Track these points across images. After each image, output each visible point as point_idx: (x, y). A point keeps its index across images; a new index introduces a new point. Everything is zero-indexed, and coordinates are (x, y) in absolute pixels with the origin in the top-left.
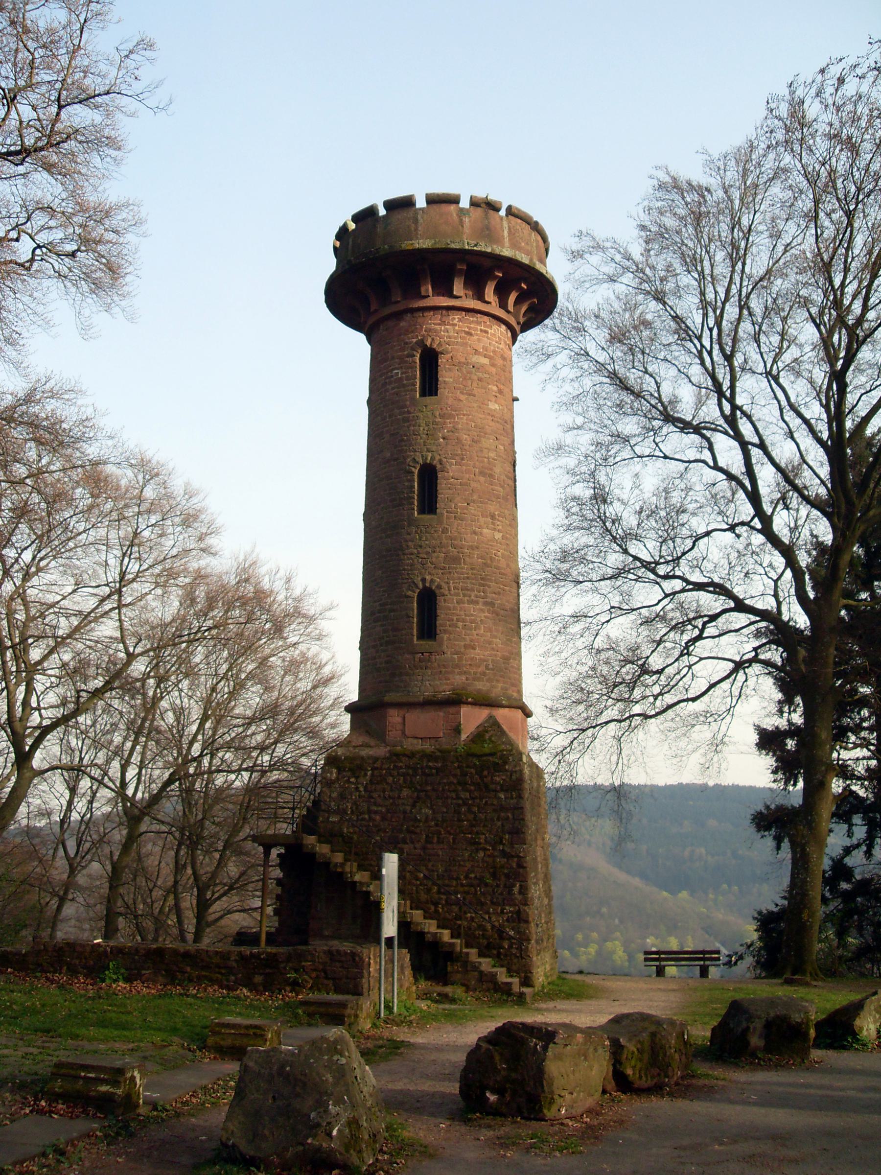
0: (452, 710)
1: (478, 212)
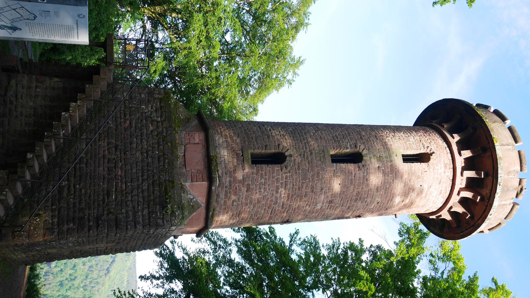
0: (205, 176)
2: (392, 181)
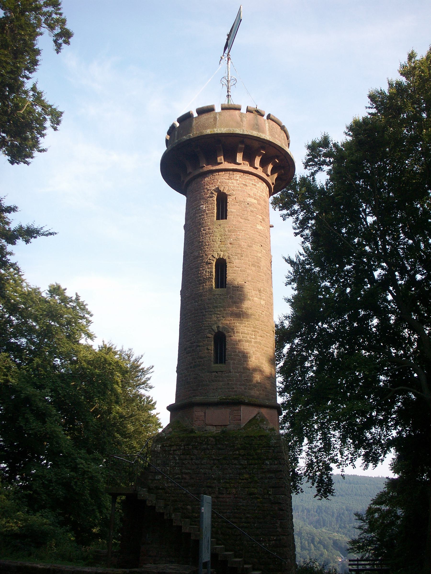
1: (251, 116)
2: (243, 232)
